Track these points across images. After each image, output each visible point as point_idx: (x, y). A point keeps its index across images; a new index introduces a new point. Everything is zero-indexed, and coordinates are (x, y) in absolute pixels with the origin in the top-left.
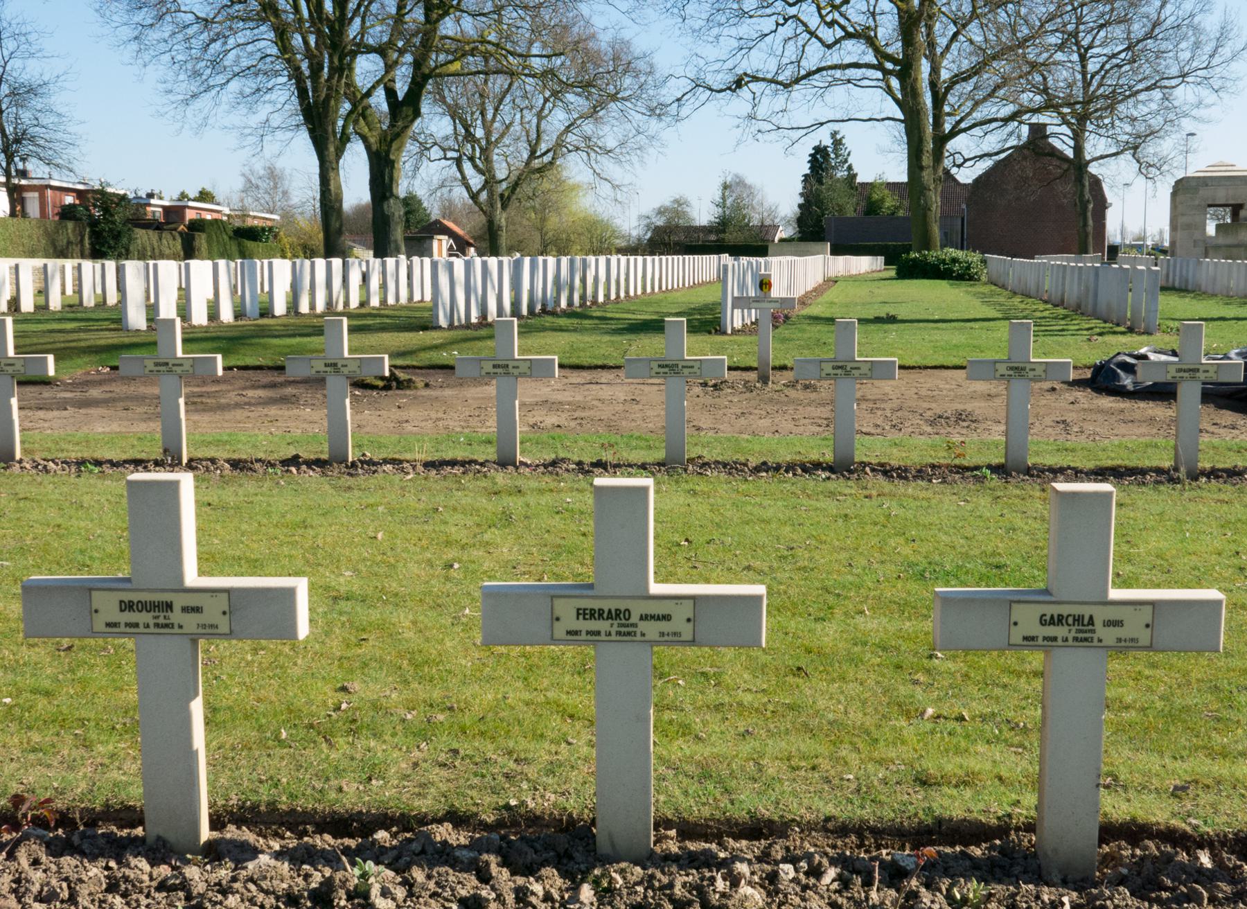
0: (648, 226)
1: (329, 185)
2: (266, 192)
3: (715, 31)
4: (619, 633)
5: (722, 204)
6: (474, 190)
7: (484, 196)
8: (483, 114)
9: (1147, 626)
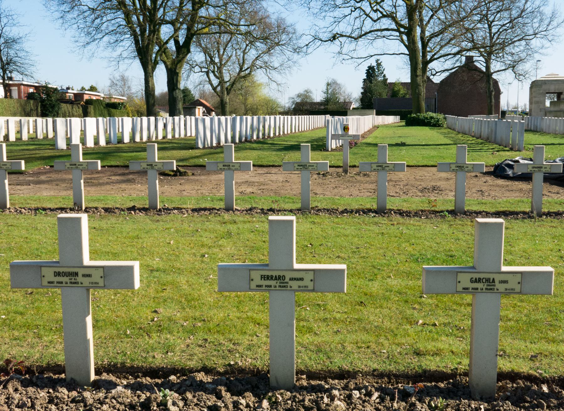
0: (293, 102)
1: (149, 83)
2: (121, 87)
3: (324, 14)
4: (280, 286)
5: (327, 92)
6: (215, 86)
7: (219, 89)
8: (218, 51)
9: (519, 283)
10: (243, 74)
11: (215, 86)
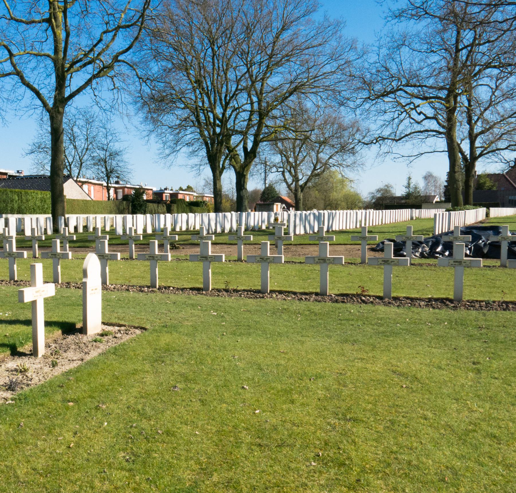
0: (373, 197)
5: (408, 186)
6: (290, 183)
7: (293, 186)
8: (294, 153)
10: (316, 172)
11: (290, 183)
